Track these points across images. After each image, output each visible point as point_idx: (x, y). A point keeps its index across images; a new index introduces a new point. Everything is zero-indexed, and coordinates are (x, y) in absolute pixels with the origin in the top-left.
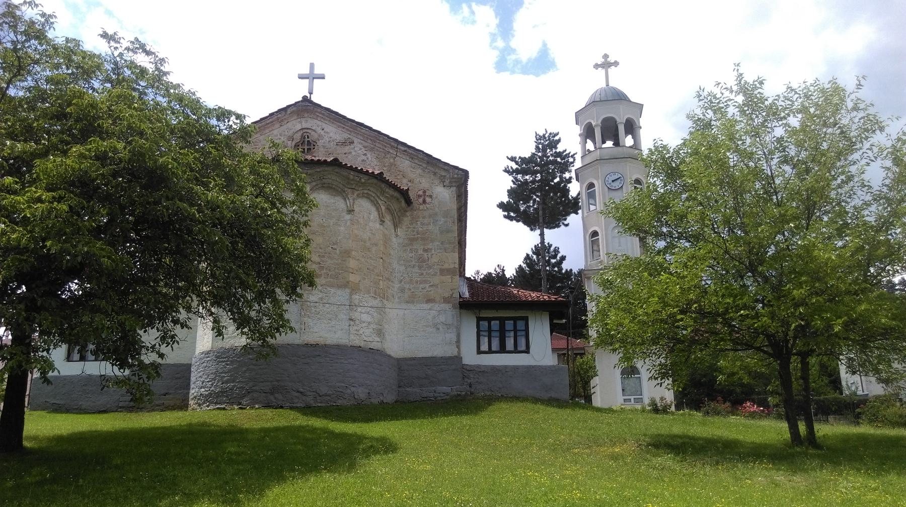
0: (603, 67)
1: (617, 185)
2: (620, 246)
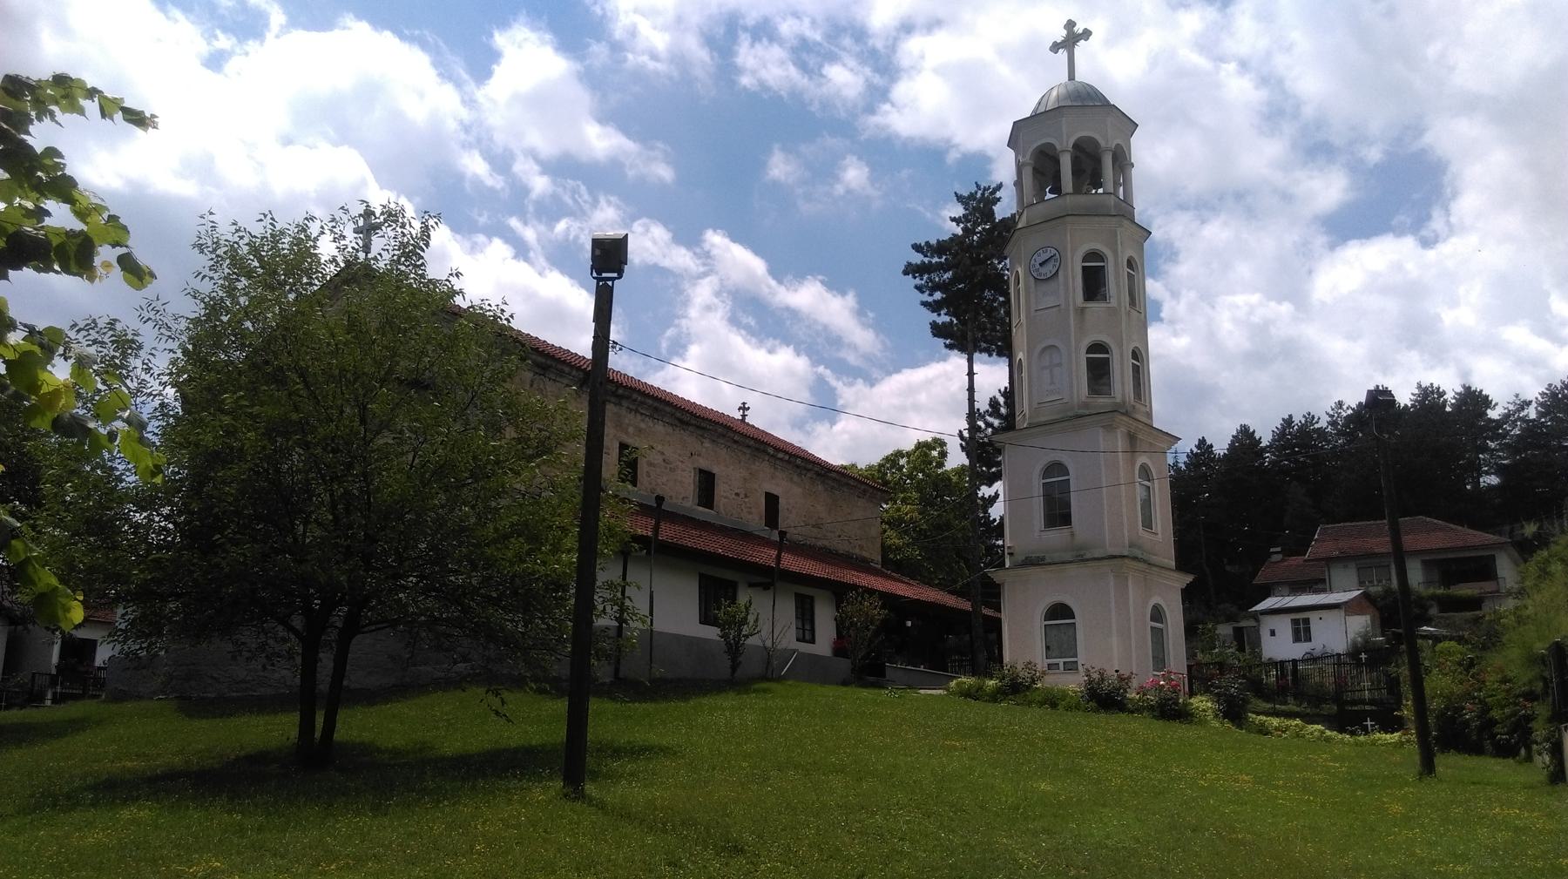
1: (1048, 270)
2: (1052, 383)
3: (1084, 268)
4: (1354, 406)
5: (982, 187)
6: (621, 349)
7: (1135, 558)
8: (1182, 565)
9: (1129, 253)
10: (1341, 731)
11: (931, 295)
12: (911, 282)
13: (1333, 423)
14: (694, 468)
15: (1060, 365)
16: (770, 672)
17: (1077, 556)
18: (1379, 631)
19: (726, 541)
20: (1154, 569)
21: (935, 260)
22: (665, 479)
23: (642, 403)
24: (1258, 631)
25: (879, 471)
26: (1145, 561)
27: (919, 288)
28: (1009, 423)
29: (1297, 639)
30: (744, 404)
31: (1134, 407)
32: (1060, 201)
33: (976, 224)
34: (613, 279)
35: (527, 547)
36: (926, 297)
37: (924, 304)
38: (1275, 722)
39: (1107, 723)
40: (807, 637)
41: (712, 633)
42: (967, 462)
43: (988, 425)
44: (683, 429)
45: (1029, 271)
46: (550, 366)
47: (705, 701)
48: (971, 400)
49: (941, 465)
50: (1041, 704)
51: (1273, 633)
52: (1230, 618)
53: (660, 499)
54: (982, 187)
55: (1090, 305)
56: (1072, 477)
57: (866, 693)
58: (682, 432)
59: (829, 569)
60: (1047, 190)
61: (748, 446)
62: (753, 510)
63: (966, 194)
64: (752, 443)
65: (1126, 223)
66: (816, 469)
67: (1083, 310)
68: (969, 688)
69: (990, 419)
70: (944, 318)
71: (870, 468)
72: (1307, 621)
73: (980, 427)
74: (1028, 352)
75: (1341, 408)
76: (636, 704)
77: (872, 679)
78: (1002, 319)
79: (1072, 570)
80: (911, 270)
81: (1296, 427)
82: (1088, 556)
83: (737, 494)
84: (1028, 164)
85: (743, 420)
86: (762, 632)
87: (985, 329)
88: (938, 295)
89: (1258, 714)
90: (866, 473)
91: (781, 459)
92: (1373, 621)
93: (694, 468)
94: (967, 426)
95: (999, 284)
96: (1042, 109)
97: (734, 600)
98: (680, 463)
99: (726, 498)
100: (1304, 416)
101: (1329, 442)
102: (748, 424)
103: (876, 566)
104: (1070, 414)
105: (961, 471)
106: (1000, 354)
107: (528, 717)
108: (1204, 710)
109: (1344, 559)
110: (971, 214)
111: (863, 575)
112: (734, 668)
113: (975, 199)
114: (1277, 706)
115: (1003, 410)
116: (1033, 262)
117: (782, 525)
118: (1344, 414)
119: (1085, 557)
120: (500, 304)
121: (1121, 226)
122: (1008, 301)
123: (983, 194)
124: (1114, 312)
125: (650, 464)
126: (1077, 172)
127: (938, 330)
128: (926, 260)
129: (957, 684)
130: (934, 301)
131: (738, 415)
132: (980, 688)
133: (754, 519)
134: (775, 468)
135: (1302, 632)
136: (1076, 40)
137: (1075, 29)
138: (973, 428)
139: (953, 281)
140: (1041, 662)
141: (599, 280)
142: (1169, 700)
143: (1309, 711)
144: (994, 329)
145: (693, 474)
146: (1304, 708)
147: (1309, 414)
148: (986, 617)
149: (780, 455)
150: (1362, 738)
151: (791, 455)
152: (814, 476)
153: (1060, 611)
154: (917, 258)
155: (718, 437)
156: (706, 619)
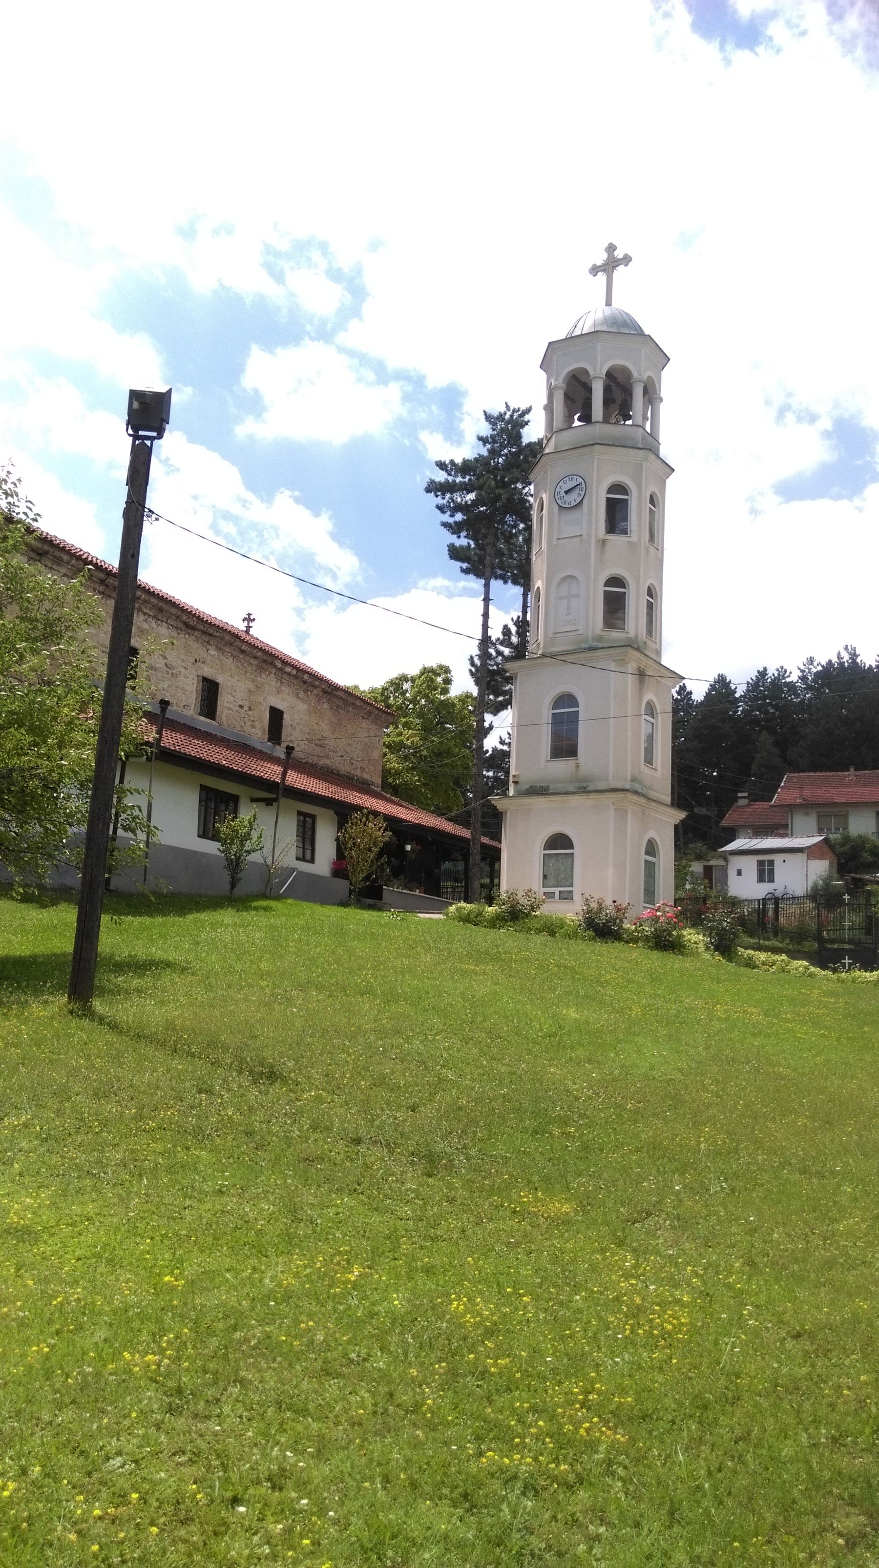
0: (604, 270)
1: (574, 498)
2: (569, 614)
3: (608, 499)
4: (824, 663)
5: (512, 408)
6: (157, 519)
7: (636, 793)
8: (679, 801)
9: (653, 488)
10: (824, 967)
11: (452, 516)
12: (434, 500)
13: (803, 678)
14: (198, 676)
15: (578, 596)
16: (268, 889)
17: (580, 788)
18: (836, 876)
19: (230, 754)
20: (653, 804)
21: (459, 479)
22: (166, 685)
23: (145, 601)
24: (726, 870)
25: (382, 694)
26: (644, 796)
27: (441, 509)
28: (520, 652)
29: (761, 879)
30: (249, 615)
31: (645, 643)
32: (589, 429)
33: (503, 446)
34: (152, 439)
35: (29, 739)
36: (446, 518)
37: (445, 525)
38: (763, 956)
39: (609, 952)
40: (308, 856)
41: (211, 847)
42: (474, 691)
43: (499, 653)
44: (189, 634)
45: (554, 498)
46: (47, 553)
47: (203, 916)
48: (485, 627)
49: (445, 691)
50: (539, 931)
51: (739, 873)
52: (699, 857)
53: (164, 704)
54: (512, 408)
55: (612, 537)
56: (582, 709)
57: (367, 915)
58: (187, 636)
59: (333, 788)
60: (576, 417)
61: (255, 657)
62: (256, 723)
63: (496, 414)
64: (259, 654)
65: (652, 457)
66: (324, 686)
67: (604, 542)
68: (468, 914)
69: (501, 648)
70: (462, 541)
71: (373, 691)
72: (771, 863)
73: (491, 655)
74: (547, 581)
75: (812, 664)
76: (130, 917)
77: (369, 901)
78: (521, 546)
79: (575, 800)
80: (433, 488)
81: (769, 680)
82: (591, 788)
83: (241, 707)
84: (560, 388)
85: (247, 632)
86: (264, 850)
87: (503, 554)
88: (459, 517)
89: (746, 948)
90: (369, 696)
91: (289, 674)
92: (831, 866)
93: (198, 676)
94: (478, 653)
95: (522, 511)
96: (577, 332)
97: (235, 812)
98: (183, 670)
99: (229, 709)
100: (777, 670)
101: (797, 696)
102: (252, 636)
103: (376, 788)
104: (584, 646)
105: (465, 698)
106: (515, 582)
107: (11, 926)
108: (696, 943)
109: (807, 806)
110: (498, 434)
111: (365, 797)
112: (233, 885)
113: (503, 420)
114: (762, 941)
115: (514, 639)
116: (558, 489)
117: (286, 742)
118: (814, 670)
119: (588, 789)
120: (6, 465)
121: (646, 460)
122: (529, 528)
123: (512, 416)
124: (633, 546)
125: (151, 668)
126: (608, 401)
127: (455, 553)
128: (450, 479)
129: (457, 909)
130: (455, 522)
131: (242, 626)
132: (480, 914)
133: (258, 734)
134: (282, 683)
135: (766, 873)
136: (615, 264)
137: (616, 253)
138: (484, 655)
139: (475, 503)
140: (539, 890)
141: (135, 437)
142: (664, 931)
143: (790, 947)
144: (511, 557)
145: (195, 682)
146: (786, 944)
147: (782, 668)
148: (483, 846)
149: (288, 669)
150: (843, 975)
151: (298, 669)
152: (321, 694)
153: (560, 841)
154: (441, 476)
155: (225, 645)
156: (206, 831)
